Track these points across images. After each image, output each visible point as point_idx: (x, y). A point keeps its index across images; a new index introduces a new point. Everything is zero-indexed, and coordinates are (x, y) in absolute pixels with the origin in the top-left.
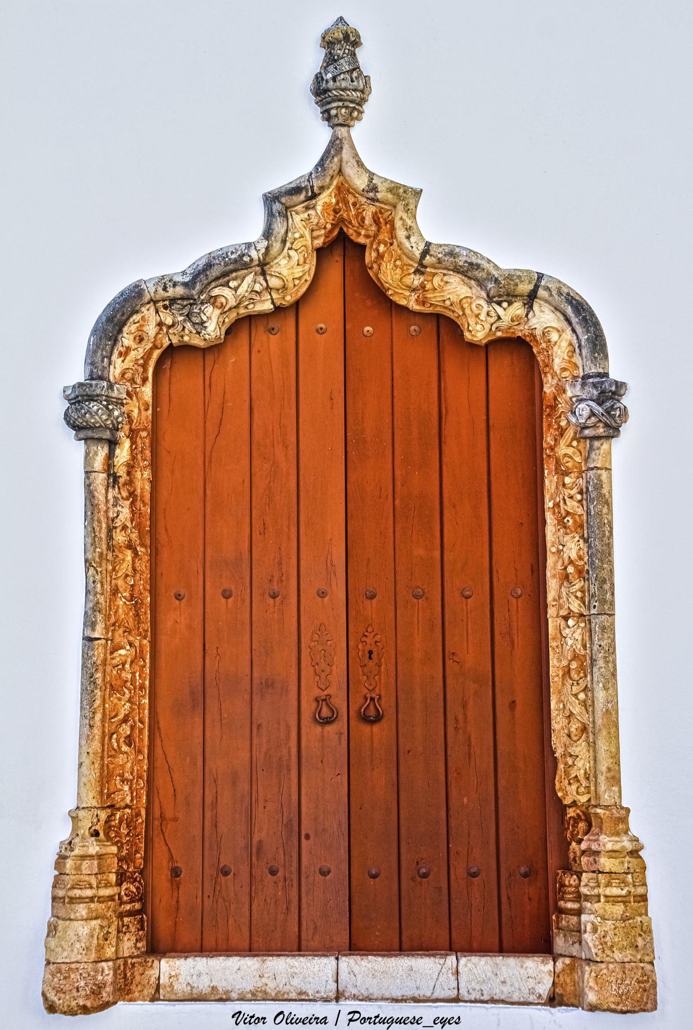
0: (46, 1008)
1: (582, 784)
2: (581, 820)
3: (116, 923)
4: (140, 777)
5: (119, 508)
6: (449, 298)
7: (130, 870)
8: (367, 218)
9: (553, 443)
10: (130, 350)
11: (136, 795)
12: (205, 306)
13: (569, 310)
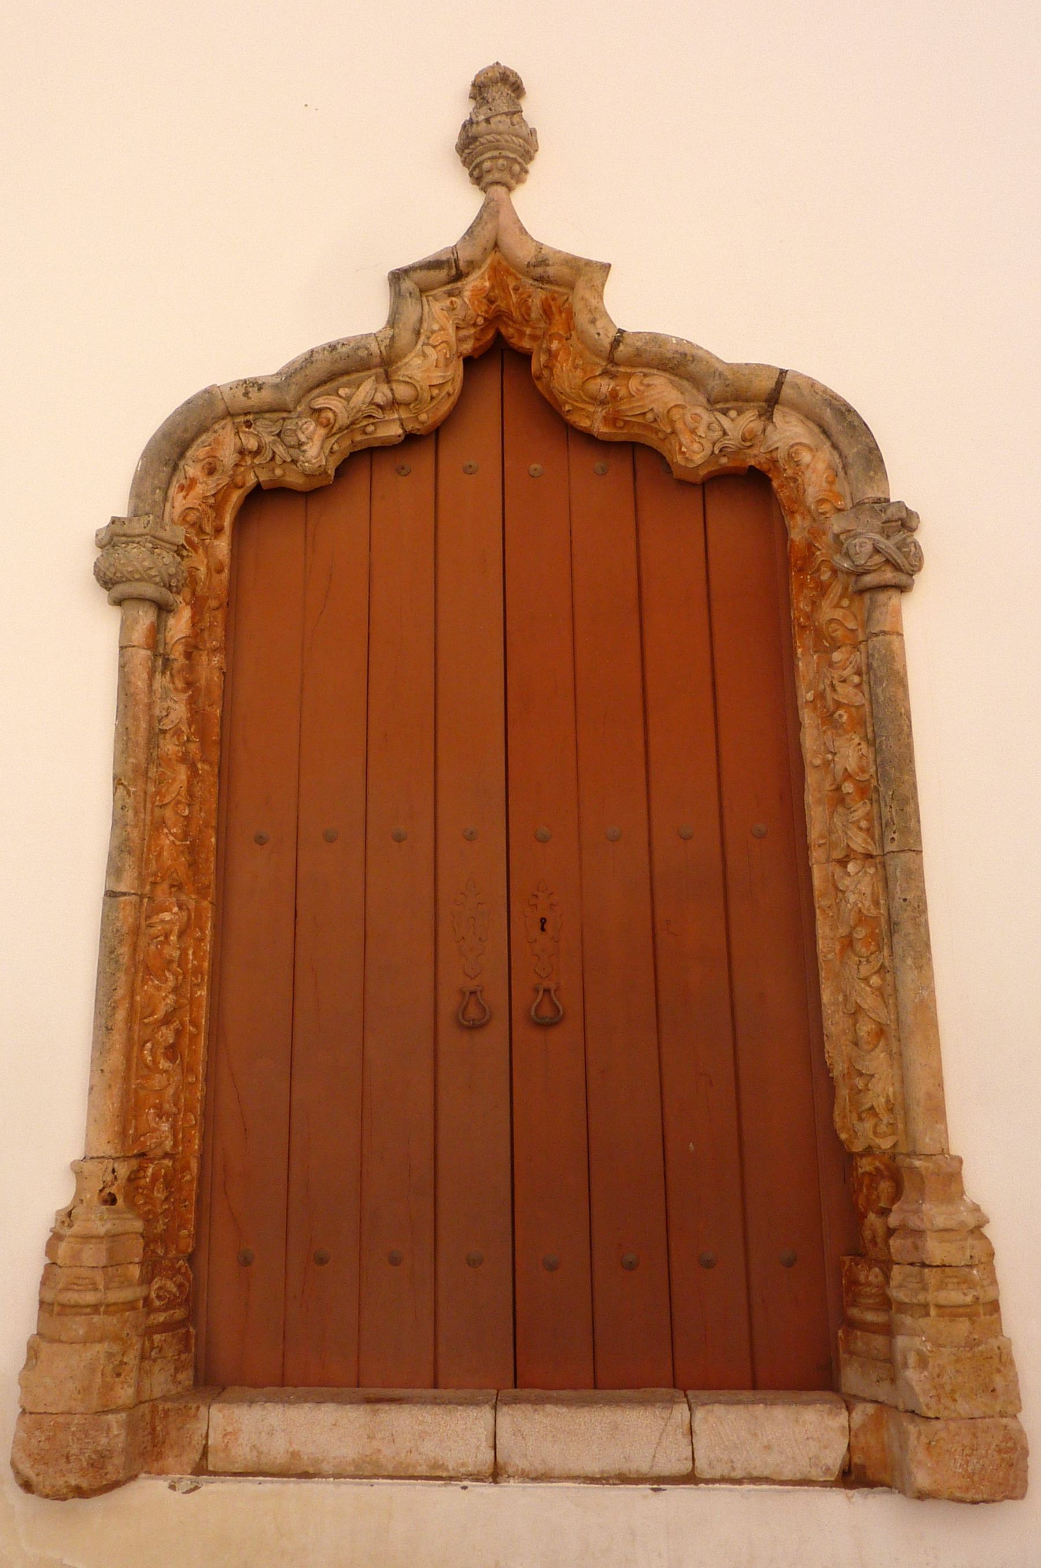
0: (21, 1485)
1: (881, 1120)
2: (883, 1177)
3: (138, 1346)
4: (189, 1109)
5: (170, 703)
6: (652, 409)
7: (170, 1255)
8: (533, 309)
9: (808, 609)
10: (196, 483)
11: (183, 1138)
12: (304, 421)
13: (828, 415)
